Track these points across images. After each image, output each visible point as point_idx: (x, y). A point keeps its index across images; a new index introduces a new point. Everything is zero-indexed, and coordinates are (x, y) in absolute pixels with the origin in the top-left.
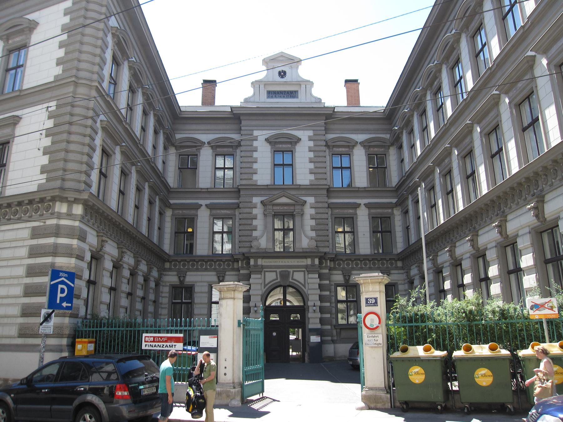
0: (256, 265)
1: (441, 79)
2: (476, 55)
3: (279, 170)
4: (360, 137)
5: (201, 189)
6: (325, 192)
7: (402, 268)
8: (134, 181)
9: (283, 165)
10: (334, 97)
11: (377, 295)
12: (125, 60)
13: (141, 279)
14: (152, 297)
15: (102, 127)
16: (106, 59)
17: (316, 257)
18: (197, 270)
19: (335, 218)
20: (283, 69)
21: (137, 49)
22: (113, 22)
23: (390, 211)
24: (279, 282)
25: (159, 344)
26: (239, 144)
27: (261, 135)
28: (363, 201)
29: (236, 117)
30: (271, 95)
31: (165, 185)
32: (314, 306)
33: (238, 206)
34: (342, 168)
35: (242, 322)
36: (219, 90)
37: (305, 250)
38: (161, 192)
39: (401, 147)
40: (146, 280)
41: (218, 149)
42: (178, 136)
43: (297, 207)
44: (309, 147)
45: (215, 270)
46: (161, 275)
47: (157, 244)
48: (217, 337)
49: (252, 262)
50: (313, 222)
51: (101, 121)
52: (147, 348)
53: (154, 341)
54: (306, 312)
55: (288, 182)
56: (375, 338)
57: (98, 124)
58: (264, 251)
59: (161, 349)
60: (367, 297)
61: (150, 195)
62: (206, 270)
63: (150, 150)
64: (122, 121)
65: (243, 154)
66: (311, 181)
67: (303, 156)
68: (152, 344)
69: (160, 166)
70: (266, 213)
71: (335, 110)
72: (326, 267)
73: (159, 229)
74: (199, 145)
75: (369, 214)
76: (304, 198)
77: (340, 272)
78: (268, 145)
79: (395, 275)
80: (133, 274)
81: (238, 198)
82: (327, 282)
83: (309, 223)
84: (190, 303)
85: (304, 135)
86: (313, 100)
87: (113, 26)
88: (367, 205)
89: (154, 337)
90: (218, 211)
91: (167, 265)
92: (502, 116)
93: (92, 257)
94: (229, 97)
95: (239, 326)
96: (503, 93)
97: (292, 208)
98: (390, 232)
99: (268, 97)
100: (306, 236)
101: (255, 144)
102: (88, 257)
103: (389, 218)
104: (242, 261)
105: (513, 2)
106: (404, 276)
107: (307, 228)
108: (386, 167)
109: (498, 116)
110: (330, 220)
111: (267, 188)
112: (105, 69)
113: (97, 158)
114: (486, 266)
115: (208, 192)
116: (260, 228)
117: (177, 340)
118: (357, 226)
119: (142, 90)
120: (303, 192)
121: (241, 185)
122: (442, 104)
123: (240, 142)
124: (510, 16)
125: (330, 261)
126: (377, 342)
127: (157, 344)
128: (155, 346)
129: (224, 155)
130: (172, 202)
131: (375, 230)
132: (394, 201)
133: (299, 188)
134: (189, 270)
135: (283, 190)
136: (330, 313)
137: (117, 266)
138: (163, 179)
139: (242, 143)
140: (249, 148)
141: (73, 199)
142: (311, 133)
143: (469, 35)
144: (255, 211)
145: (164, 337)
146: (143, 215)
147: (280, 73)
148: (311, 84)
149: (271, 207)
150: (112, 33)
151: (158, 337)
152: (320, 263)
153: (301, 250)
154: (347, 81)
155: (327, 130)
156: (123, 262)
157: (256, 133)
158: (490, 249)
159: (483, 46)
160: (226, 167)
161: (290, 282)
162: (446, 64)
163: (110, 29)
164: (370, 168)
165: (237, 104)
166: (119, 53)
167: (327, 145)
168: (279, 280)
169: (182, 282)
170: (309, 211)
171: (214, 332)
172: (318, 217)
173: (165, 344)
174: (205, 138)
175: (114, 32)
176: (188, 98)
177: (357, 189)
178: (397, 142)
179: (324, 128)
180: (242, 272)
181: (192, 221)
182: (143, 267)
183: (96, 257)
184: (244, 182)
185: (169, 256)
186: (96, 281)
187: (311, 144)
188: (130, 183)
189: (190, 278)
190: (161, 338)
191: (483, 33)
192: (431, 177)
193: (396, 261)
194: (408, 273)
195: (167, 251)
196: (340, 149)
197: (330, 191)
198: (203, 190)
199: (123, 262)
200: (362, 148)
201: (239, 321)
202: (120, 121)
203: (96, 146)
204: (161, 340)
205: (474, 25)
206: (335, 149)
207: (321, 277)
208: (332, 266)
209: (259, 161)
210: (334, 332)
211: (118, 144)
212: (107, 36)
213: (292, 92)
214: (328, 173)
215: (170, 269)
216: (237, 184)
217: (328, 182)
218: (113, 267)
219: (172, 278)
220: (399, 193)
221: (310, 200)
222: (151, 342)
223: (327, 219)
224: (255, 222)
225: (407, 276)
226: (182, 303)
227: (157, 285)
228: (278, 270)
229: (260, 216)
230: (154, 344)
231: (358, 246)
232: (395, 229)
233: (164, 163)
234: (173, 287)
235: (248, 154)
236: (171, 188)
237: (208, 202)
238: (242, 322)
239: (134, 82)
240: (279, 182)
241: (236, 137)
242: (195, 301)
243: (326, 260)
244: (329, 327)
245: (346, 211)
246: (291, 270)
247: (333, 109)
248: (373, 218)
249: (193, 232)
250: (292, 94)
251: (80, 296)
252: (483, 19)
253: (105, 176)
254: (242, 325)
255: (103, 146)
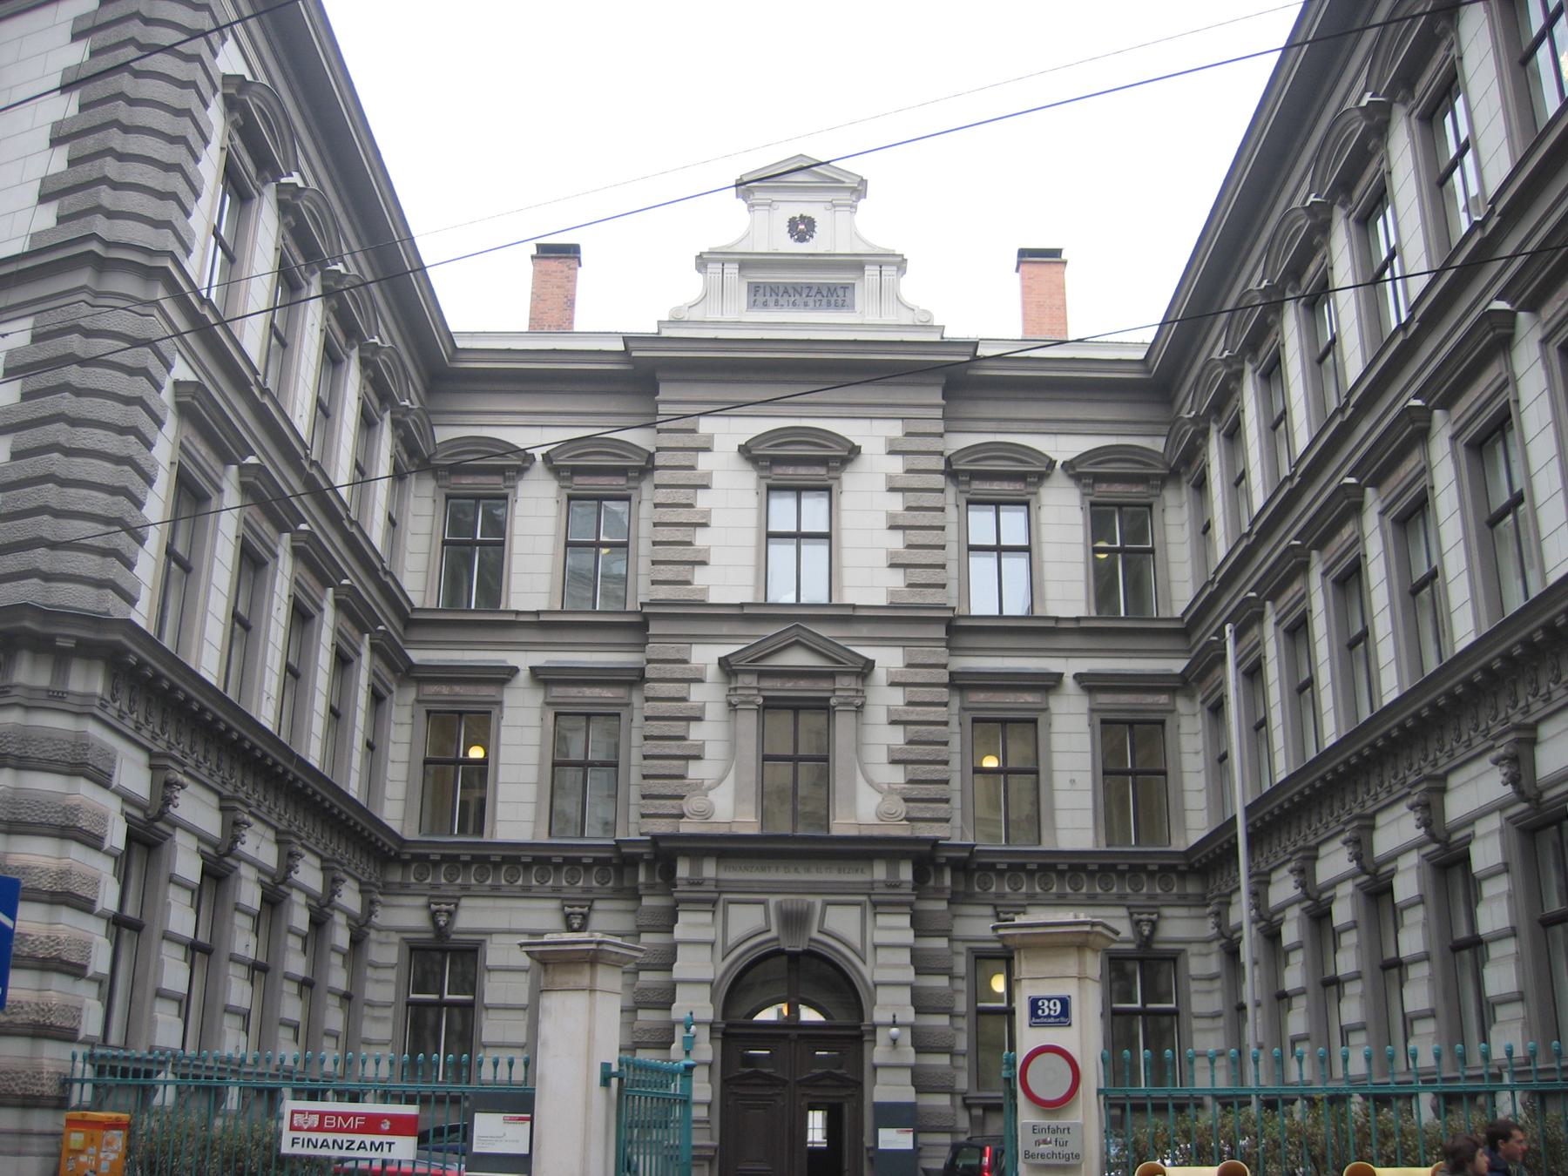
0: (696, 883)
1: (1328, 255)
2: (1439, 181)
3: (782, 554)
4: (1063, 448)
5: (517, 613)
6: (940, 632)
7: (1202, 902)
8: (286, 585)
9: (799, 536)
10: (975, 307)
11: (1068, 989)
12: (265, 182)
13: (300, 918)
14: (338, 978)
15: (178, 404)
16: (203, 182)
17: (904, 856)
18: (495, 893)
19: (975, 721)
20: (807, 210)
21: (309, 142)
22: (229, 60)
23: (1163, 699)
24: (776, 939)
25: (340, 1137)
26: (647, 467)
27: (727, 434)
28: (1069, 667)
29: (642, 374)
30: (761, 299)
31: (393, 596)
32: (894, 1024)
33: (635, 679)
34: (999, 549)
35: (615, 1068)
36: (588, 279)
37: (866, 832)
38: (379, 623)
39: (1201, 485)
40: (319, 922)
41: (578, 480)
42: (443, 434)
43: (842, 682)
44: (889, 478)
45: (555, 894)
46: (369, 906)
47: (363, 801)
48: (532, 1120)
49: (683, 870)
50: (897, 736)
51: (177, 383)
52: (298, 1150)
53: (320, 1129)
54: (867, 1046)
55: (815, 592)
56: (1059, 1136)
57: (167, 395)
58: (723, 830)
59: (344, 1153)
60: (1036, 993)
61: (338, 632)
62: (527, 893)
63: (342, 473)
64: (247, 384)
65: (662, 496)
66: (892, 593)
67: (868, 501)
68: (314, 1136)
69: (377, 534)
70: (734, 700)
71: (981, 352)
72: (938, 893)
73: (370, 746)
74: (514, 464)
75: (1092, 711)
76: (867, 652)
77: (989, 911)
78: (749, 467)
79: (1178, 922)
80: (273, 900)
81: (641, 647)
82: (942, 943)
83: (884, 737)
84: (470, 1006)
85: (872, 436)
86: (906, 319)
87: (229, 72)
88: (1090, 684)
89: (322, 1115)
90: (573, 691)
91: (396, 876)
92: (1522, 385)
93: (130, 838)
94: (621, 303)
95: (605, 1082)
96: (1521, 309)
97: (825, 685)
98: (1165, 773)
99: (753, 305)
100: (871, 783)
101: (704, 462)
102: (116, 837)
103: (1162, 723)
104: (650, 865)
105: (1552, 6)
106: (1209, 928)
107: (877, 755)
108: (1152, 551)
109: (1505, 384)
110: (954, 726)
111: (742, 615)
112: (195, 212)
113: (157, 503)
114: (1473, 896)
115: (542, 626)
116: (715, 751)
117: (401, 1126)
118: (1049, 752)
119: (323, 278)
120: (865, 630)
121: (653, 603)
122: (1334, 340)
123: (651, 456)
124: (1543, 52)
125: (954, 870)
126: (1067, 1150)
127: (330, 1137)
128: (325, 1144)
129: (799, 490)
130: (416, 656)
131: (1112, 767)
132: (1178, 666)
133: (849, 616)
134: (467, 892)
135: (797, 622)
136: (950, 1050)
137: (218, 871)
138: (388, 579)
139: (660, 460)
140: (682, 477)
141: (70, 644)
142: (895, 429)
143: (1416, 112)
144: (697, 694)
145: (355, 1115)
146: (313, 698)
147: (793, 223)
148: (900, 263)
149: (751, 680)
150: (225, 96)
151: (337, 1114)
152: (920, 877)
153: (853, 832)
154: (1026, 255)
155: (952, 422)
156: (239, 859)
157: (706, 425)
158: (1486, 836)
159: (1463, 149)
160: (804, 529)
161: (811, 940)
162: (1343, 205)
163: (218, 82)
164: (1096, 550)
165: (650, 328)
166: (247, 159)
167: (951, 473)
168: (774, 933)
169: (1146, 942)
170: (884, 699)
171: (518, 1101)
172: (913, 717)
173: (358, 1138)
174: (534, 438)
175: (233, 91)
176: (481, 302)
177: (1051, 624)
178: (1185, 468)
179: (939, 413)
180: (646, 901)
181: (482, 723)
182: (309, 874)
183: (147, 839)
184: (663, 593)
185: (403, 842)
186: (145, 920)
187: (896, 465)
188: (272, 591)
189: (472, 916)
190: (346, 1116)
191: (1459, 104)
192: (1296, 586)
193: (1183, 876)
194: (1221, 916)
195: (395, 826)
196: (996, 486)
197: (960, 630)
198: (522, 618)
199: (239, 859)
200: (1071, 483)
201: (606, 1066)
202: (240, 383)
203: (155, 465)
204: (342, 1124)
205: (1427, 82)
206: (977, 485)
207: (920, 926)
208: (961, 888)
209: (714, 522)
210: (963, 1121)
211: (227, 459)
212: (206, 106)
213: (832, 290)
214: (952, 568)
215: (403, 889)
216: (642, 599)
217: (950, 597)
218: (203, 873)
219: (407, 915)
220: (1193, 640)
221: (887, 659)
222: (310, 1130)
223: (946, 723)
224: (696, 732)
225: (1218, 926)
226: (440, 1004)
227: (357, 941)
228: (773, 900)
229: (715, 710)
230: (321, 1137)
231: (1053, 819)
232: (1179, 763)
233: (392, 522)
234: (412, 949)
235: (680, 496)
236: (414, 610)
237: (540, 659)
238: (615, 1068)
239: (296, 252)
240: (783, 593)
241: (639, 438)
242: (488, 999)
243: (939, 869)
244: (943, 1100)
245: (1010, 698)
246: (818, 901)
247: (971, 350)
248: (1108, 727)
249: (483, 762)
250: (836, 296)
251: (84, 967)
252: (1461, 58)
253: (186, 568)
254: (614, 1081)
255: (181, 467)
